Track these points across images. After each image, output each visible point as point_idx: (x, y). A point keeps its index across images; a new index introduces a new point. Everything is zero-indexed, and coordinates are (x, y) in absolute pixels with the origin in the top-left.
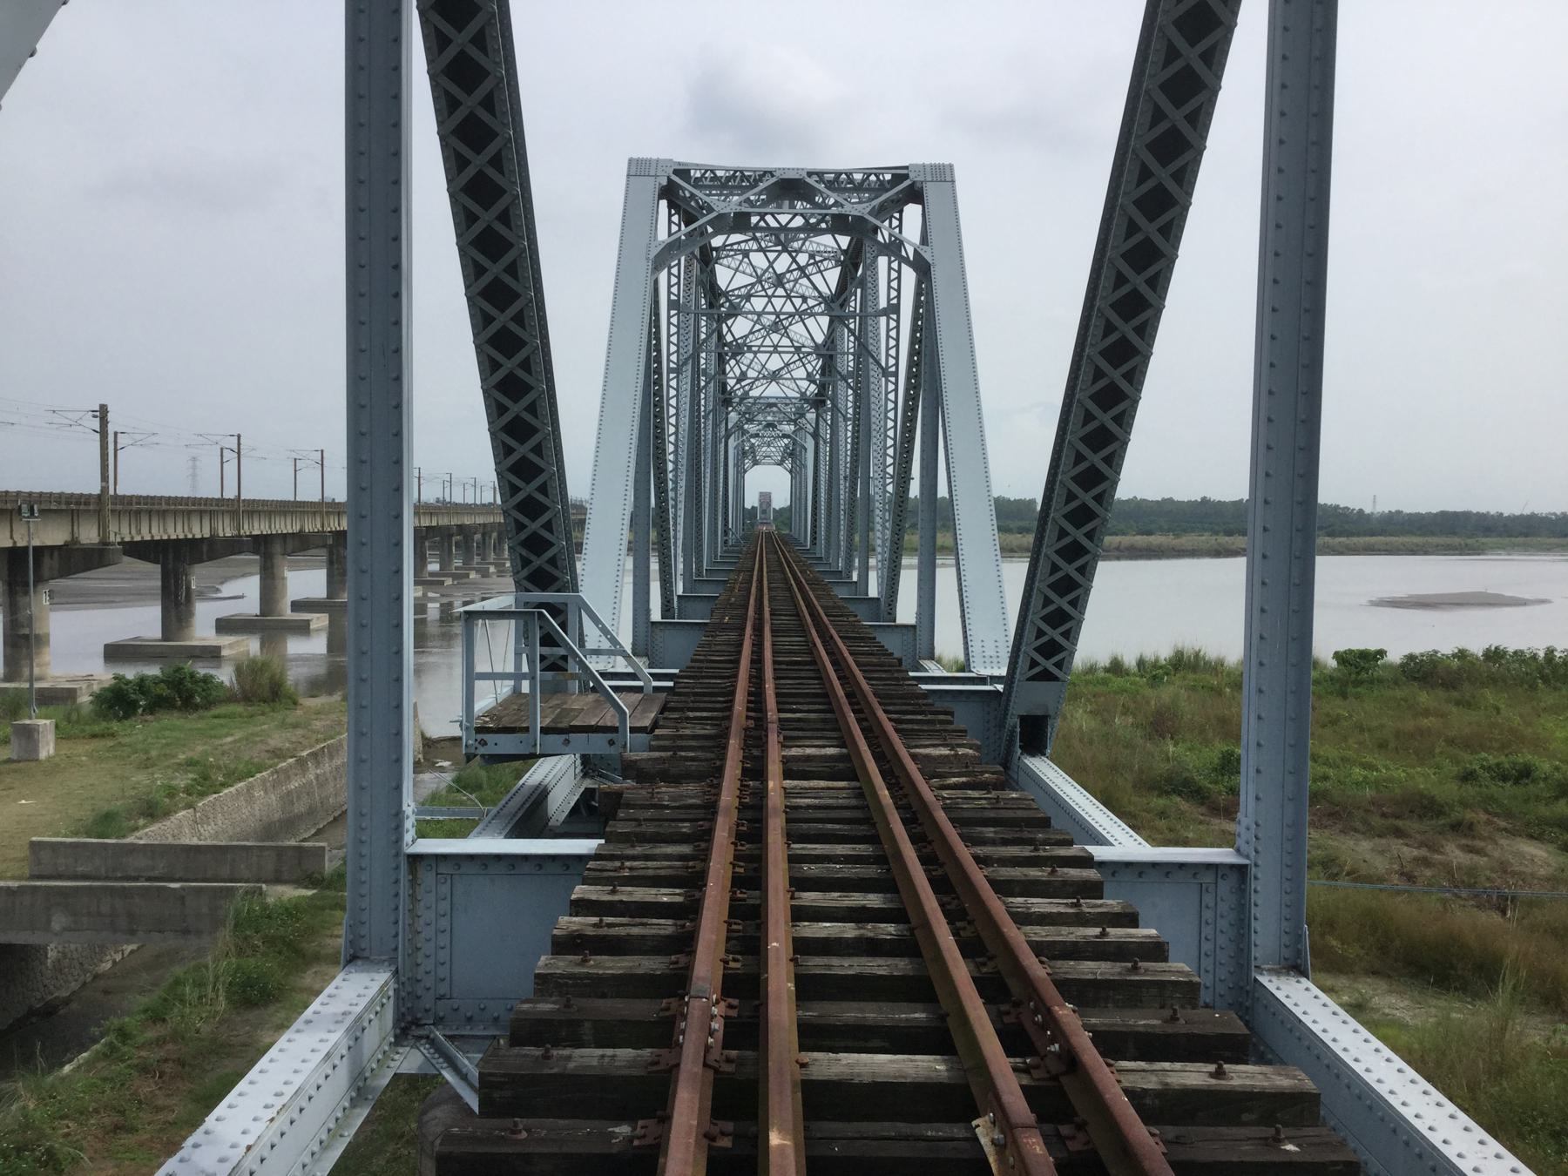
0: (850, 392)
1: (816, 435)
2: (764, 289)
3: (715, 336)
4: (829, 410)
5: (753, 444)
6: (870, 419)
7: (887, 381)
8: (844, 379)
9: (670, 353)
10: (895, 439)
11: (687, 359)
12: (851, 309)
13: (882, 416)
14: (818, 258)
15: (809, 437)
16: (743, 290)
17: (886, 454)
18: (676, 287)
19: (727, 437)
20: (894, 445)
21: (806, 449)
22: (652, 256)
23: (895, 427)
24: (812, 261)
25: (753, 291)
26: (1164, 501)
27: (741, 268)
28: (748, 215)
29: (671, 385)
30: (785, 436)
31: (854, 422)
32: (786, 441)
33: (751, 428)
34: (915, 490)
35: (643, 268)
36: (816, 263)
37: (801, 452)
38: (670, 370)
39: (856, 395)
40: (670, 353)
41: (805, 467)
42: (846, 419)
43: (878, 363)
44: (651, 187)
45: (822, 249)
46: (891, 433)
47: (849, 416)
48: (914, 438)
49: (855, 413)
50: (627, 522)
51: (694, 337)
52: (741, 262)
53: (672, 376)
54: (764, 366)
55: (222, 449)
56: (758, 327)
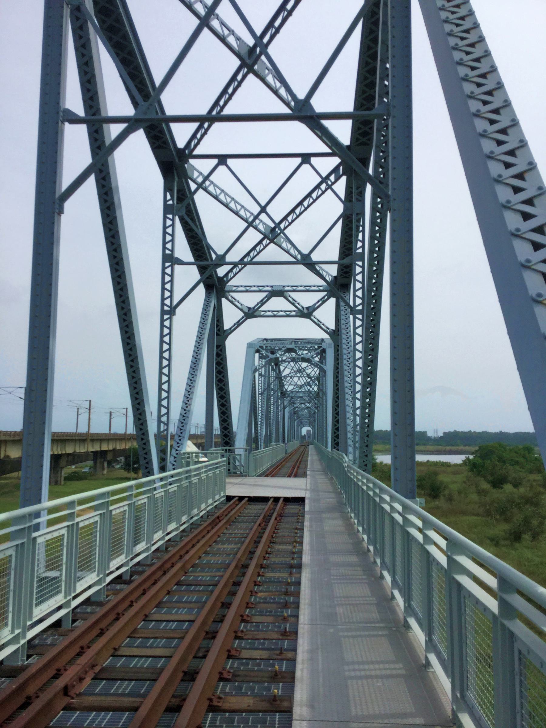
3: (283, 404)
6: (346, 434)
9: (259, 389)
10: (363, 283)
13: (352, 348)
17: (355, 366)
19: (284, 408)
20: (363, 288)
23: (363, 272)
26: (483, 432)
27: (288, 367)
29: (259, 399)
35: (250, 373)
38: (259, 394)
40: (259, 389)
43: (348, 304)
44: (253, 350)
46: (358, 285)
50: (245, 441)
52: (288, 365)
53: (260, 396)
54: (263, 209)
55: (78, 409)
56: (293, 371)
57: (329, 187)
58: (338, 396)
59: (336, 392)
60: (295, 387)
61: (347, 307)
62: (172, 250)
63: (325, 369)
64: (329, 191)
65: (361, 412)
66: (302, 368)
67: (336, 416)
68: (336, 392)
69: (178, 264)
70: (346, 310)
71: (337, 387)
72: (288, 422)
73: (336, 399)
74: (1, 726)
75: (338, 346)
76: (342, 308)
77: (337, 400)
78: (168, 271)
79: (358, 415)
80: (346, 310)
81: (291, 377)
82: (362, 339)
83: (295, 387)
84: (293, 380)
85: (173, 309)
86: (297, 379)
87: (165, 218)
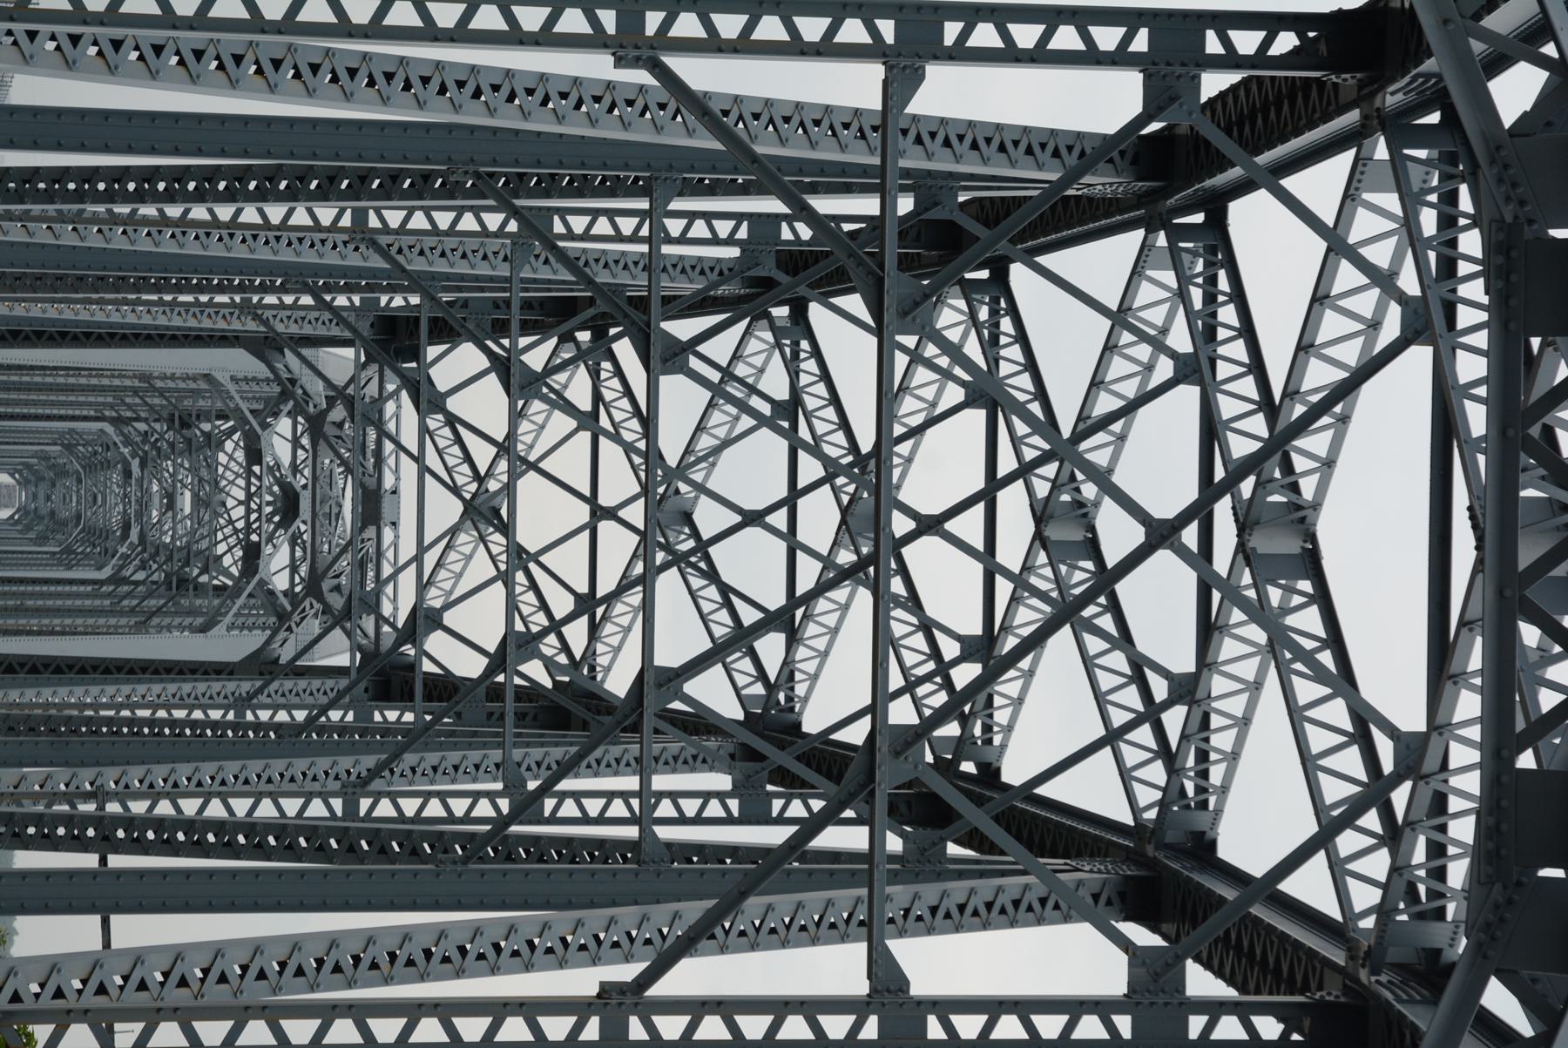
0: (300, 715)
1: (262, 666)
2: (1024, 471)
4: (364, 716)
5: (220, 446)
7: (578, 1008)
8: (527, 807)
11: (266, 323)
12: (777, 804)
14: (1174, 720)
15: (249, 643)
16: (1025, 381)
18: (619, 220)
19: (265, 346)
21: (204, 629)
22: (213, 373)
24: (1160, 690)
25: (1021, 428)
28: (260, 463)
30: (252, 555)
31: (341, 833)
32: (231, 562)
33: (281, 439)
34: (26, 859)
36: (1152, 714)
37: (192, 612)
39: (295, 729)
41: (141, 627)
42: (354, 788)
45: (1222, 741)
47: (365, 804)
48: (146, 853)
49: (379, 836)
51: (477, 278)
57: (703, 546)
58: (15, 672)
59: (49, 665)
60: (483, 454)
61: (332, 695)
62: (962, 54)
63: (215, 631)
64: (713, 551)
65: (162, 720)
66: (1106, 580)
67: (28, 667)
68: (49, 665)
69: (886, 83)
70: (325, 693)
71: (114, 670)
72: (120, 374)
73: (129, 666)
74: (18, 1014)
75: (231, 673)
76: (330, 683)
77: (51, 669)
78: (1107, 38)
79: (153, 714)
80: (325, 693)
81: (791, 408)
82: (392, 723)
83: (483, 454)
84: (762, 421)
85: (646, 53)
86: (768, 487)
87: (1131, 19)
